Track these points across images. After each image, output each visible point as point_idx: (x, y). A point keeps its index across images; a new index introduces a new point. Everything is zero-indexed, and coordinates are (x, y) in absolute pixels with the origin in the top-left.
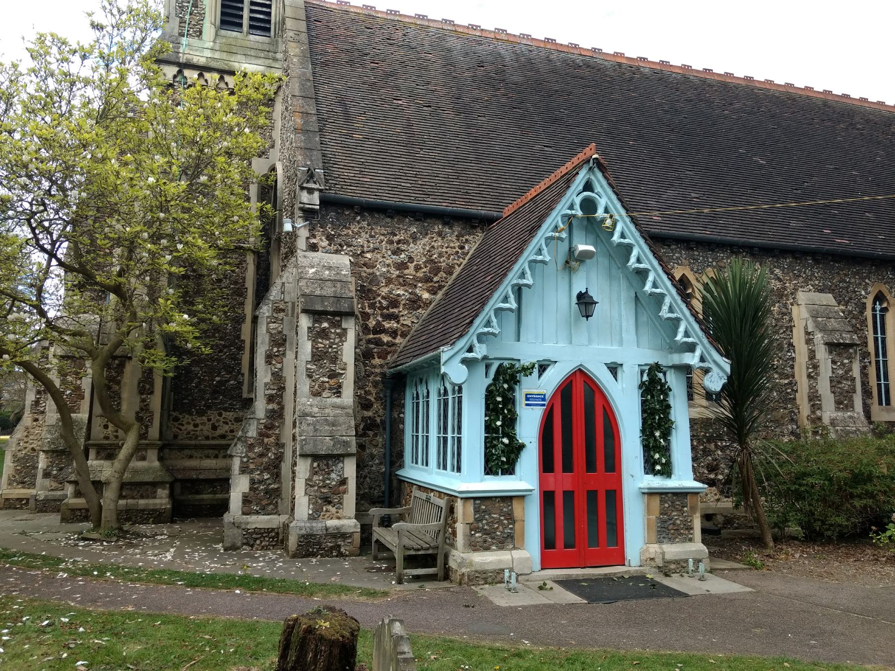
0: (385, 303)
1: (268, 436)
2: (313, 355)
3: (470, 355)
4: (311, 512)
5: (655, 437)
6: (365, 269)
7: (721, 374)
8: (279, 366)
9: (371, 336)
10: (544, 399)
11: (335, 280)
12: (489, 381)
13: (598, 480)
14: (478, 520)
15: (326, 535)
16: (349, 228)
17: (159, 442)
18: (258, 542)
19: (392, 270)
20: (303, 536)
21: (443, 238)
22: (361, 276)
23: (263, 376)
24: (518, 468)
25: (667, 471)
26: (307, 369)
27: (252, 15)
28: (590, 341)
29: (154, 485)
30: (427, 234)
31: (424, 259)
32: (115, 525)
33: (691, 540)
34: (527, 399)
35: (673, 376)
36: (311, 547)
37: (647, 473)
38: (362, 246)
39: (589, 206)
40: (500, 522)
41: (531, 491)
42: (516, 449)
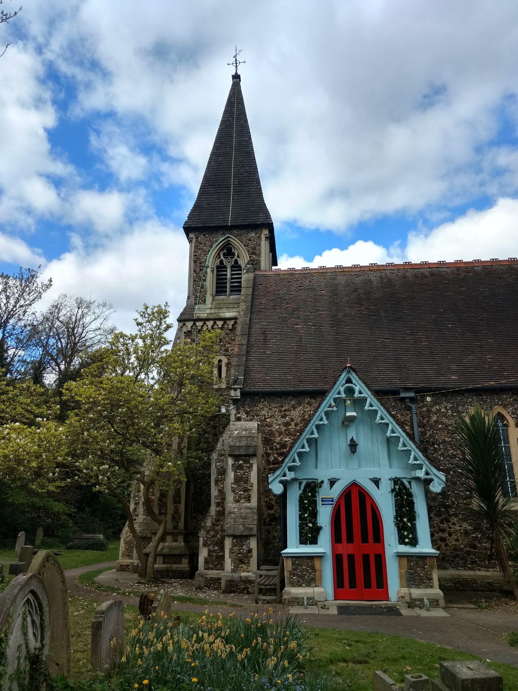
0: (278, 446)
1: (217, 526)
2: (235, 479)
3: (284, 478)
4: (233, 568)
5: (404, 522)
6: (267, 428)
7: (440, 482)
8: (222, 486)
9: (272, 466)
10: (332, 501)
11: (248, 437)
12: (301, 492)
13: (370, 548)
14: (294, 569)
15: (241, 581)
16: (258, 406)
17: (183, 531)
18: (212, 585)
19: (282, 427)
20: (228, 581)
21: (311, 406)
22: (264, 432)
23: (214, 492)
24: (319, 541)
25: (414, 542)
26: (232, 487)
27: (232, 285)
28: (360, 466)
29: (181, 556)
30: (301, 404)
31: (300, 419)
32: (153, 576)
33: (432, 587)
34: (323, 501)
35: (415, 484)
36: (233, 587)
37: (401, 544)
38: (265, 415)
39: (350, 391)
40: (307, 571)
41: (324, 553)
42: (317, 530)
